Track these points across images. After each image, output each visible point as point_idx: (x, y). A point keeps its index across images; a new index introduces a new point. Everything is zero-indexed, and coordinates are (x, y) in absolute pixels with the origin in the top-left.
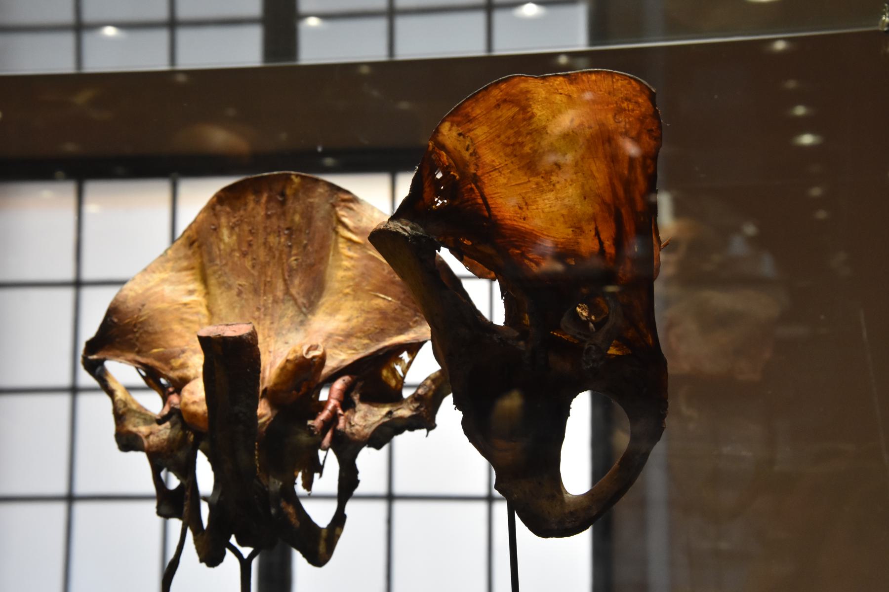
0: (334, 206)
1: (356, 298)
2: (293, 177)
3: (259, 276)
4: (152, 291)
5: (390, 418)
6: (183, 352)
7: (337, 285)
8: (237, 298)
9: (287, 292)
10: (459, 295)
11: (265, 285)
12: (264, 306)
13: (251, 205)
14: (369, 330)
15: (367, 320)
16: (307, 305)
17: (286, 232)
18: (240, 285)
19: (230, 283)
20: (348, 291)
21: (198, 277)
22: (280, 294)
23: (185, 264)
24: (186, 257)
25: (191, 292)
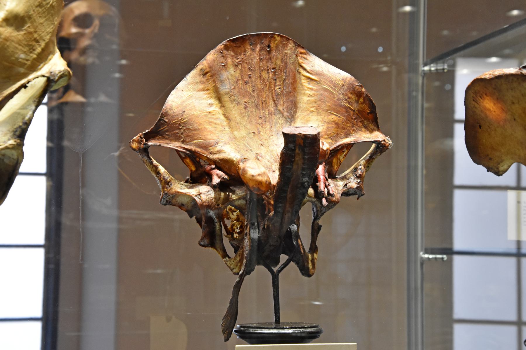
0: (297, 56)
1: (318, 114)
2: (276, 36)
4: (186, 103)
5: (346, 188)
6: (217, 143)
7: (305, 106)
8: (244, 111)
10: (157, 122)
11: (262, 103)
12: (263, 116)
14: (330, 134)
15: (328, 128)
16: (290, 117)
17: (273, 70)
18: (246, 102)
19: (239, 100)
20: (313, 109)
21: (213, 95)
23: (201, 86)
24: (202, 82)
25: (211, 105)
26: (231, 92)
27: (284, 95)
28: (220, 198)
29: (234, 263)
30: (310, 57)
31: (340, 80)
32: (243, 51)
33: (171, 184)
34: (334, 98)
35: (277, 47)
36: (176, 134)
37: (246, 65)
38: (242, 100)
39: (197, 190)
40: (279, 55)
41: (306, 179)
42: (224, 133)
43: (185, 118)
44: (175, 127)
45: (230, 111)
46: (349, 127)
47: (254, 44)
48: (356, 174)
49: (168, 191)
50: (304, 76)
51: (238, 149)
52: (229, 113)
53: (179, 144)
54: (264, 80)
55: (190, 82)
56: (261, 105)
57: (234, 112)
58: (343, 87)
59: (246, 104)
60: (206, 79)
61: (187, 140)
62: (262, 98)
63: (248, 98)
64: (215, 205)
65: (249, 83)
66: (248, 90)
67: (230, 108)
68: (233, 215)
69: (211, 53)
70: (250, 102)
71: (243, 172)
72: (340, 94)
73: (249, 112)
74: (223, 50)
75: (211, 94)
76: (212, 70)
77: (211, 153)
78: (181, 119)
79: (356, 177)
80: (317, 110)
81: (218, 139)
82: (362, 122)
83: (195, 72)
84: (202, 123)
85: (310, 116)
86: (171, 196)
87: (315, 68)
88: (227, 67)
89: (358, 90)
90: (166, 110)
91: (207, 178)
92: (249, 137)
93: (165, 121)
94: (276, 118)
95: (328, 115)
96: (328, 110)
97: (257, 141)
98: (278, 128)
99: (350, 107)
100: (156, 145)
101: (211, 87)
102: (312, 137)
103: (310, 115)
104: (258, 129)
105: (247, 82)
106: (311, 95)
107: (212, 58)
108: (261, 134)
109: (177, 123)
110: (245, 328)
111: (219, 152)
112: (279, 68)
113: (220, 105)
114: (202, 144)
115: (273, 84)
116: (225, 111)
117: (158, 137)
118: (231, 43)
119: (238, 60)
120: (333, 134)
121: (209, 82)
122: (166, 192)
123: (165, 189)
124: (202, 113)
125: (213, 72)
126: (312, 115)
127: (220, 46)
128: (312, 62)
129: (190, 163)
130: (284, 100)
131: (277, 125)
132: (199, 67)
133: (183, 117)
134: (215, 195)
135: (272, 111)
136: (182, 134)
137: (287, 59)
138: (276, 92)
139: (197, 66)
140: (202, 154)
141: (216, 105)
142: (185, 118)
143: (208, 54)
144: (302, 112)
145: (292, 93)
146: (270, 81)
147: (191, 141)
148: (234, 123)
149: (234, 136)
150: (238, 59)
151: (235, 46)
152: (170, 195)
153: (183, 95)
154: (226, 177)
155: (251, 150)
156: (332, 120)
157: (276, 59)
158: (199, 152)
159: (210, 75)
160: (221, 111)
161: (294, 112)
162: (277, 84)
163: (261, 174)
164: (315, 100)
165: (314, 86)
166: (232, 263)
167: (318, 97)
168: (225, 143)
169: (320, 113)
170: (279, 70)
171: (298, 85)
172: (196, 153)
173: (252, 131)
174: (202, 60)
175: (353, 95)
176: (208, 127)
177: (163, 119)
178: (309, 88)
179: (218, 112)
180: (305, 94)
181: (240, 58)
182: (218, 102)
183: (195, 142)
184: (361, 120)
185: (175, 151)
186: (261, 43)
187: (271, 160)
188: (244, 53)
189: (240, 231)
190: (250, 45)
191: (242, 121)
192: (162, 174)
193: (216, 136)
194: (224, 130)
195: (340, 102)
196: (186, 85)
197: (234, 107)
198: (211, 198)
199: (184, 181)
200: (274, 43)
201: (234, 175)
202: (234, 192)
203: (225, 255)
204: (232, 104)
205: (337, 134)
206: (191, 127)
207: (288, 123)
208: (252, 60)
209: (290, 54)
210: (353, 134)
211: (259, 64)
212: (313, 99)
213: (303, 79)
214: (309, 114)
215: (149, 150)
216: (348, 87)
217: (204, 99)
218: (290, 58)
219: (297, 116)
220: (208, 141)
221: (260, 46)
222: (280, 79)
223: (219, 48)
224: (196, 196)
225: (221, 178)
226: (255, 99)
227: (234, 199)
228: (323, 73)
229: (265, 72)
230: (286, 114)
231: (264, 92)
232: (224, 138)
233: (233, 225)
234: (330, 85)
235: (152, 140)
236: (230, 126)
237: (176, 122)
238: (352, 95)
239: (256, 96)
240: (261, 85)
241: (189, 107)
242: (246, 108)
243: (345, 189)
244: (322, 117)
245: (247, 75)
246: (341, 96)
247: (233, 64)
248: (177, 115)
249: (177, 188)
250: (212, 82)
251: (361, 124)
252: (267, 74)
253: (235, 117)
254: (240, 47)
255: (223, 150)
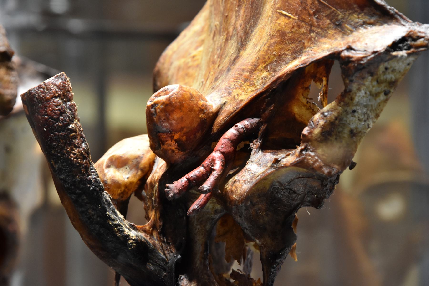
14: (269, 58)
120: (272, 57)
184: (328, 12)
205: (279, 55)
251: (328, 21)
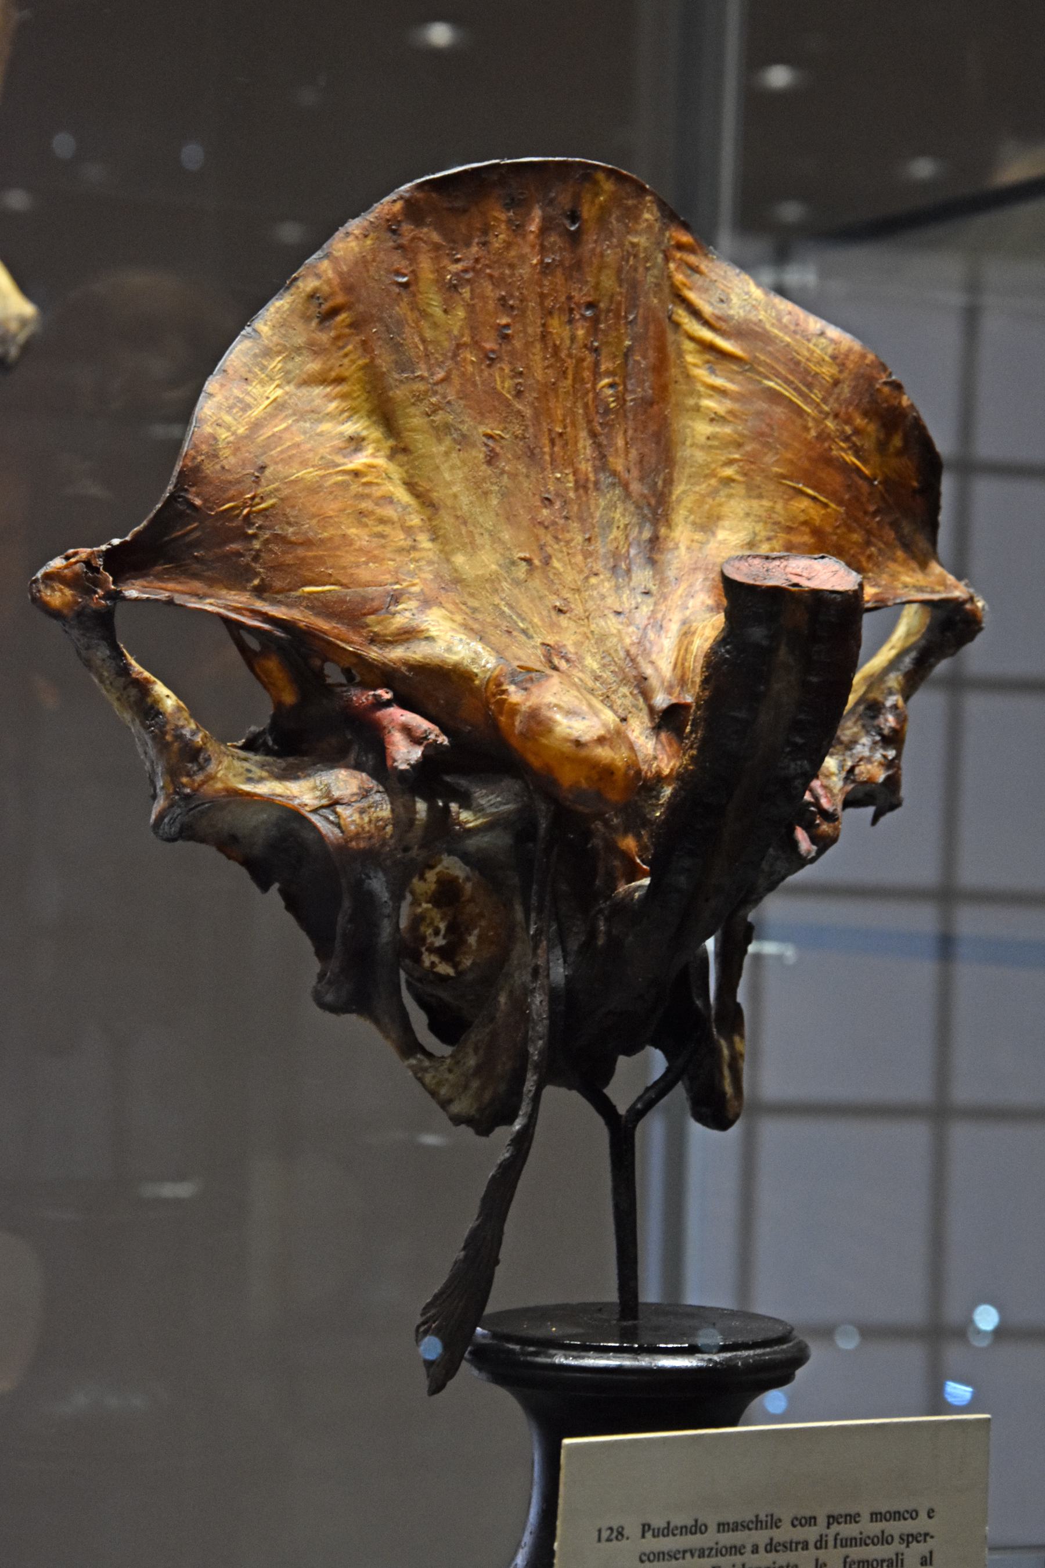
0: (667, 259)
2: (601, 176)
3: (537, 416)
4: (267, 432)
6: (396, 598)
7: (700, 456)
9: (602, 462)
10: (159, 506)
11: (553, 443)
12: (558, 495)
13: (500, 237)
16: (653, 502)
17: (588, 313)
18: (490, 437)
19: (464, 428)
20: (729, 472)
22: (586, 467)
23: (314, 366)
24: (315, 349)
25: (356, 443)
26: (435, 393)
27: (628, 414)
28: (412, 821)
29: (451, 1077)
30: (710, 265)
31: (823, 360)
32: (478, 229)
33: (208, 760)
34: (807, 429)
35: (602, 220)
36: (234, 559)
37: (488, 289)
38: (476, 428)
39: (315, 788)
40: (609, 252)
41: (801, 766)
42: (417, 561)
43: (270, 495)
44: (229, 528)
45: (433, 470)
46: (854, 543)
47: (518, 204)
48: (881, 729)
49: (196, 785)
50: (692, 338)
51: (476, 626)
52: (430, 480)
53: (243, 599)
54: (556, 350)
55: (271, 345)
56: (547, 449)
57: (447, 476)
58: (837, 390)
59: (490, 443)
60: (332, 334)
61: (278, 584)
62: (552, 421)
63: (500, 422)
64: (396, 849)
65: (499, 359)
66: (499, 387)
67: (432, 457)
68: (425, 880)
69: (350, 230)
70: (507, 436)
71: (533, 724)
72: (827, 414)
73: (505, 476)
74: (399, 222)
75: (355, 399)
76: (358, 301)
77: (374, 640)
78: (253, 498)
79: (878, 738)
80: (745, 475)
81: (396, 583)
82: (895, 525)
83: (287, 306)
84: (331, 517)
85: (723, 499)
86: (207, 805)
87: (730, 308)
88: (419, 291)
89: (887, 401)
90: (194, 458)
91: (349, 737)
92: (513, 579)
93: (192, 506)
94: (602, 503)
95: (786, 497)
96: (784, 477)
97: (541, 594)
98: (615, 545)
99: (858, 469)
100: (157, 600)
101: (354, 367)
102: (842, 601)
103: (722, 493)
104: (542, 548)
105: (492, 356)
106: (722, 417)
107: (357, 249)
108: (554, 568)
109: (237, 512)
110: (530, 1345)
111: (409, 635)
112: (611, 302)
113: (391, 442)
114: (335, 603)
115: (588, 369)
116: (411, 471)
117: (160, 568)
118: (434, 195)
119: (459, 266)
121: (346, 350)
122: (188, 791)
123: (184, 780)
124: (330, 474)
125: (361, 308)
126: (730, 496)
127: (388, 205)
128: (717, 284)
129: (281, 676)
130: (630, 432)
131: (611, 532)
132: (300, 283)
133: (260, 490)
134: (393, 810)
135: (586, 474)
136: (256, 558)
137: (636, 270)
138: (601, 400)
139: (296, 279)
140: (338, 642)
141: (374, 445)
142: (270, 495)
143: (340, 234)
144: (692, 481)
145: (656, 407)
146: (579, 354)
147: (290, 590)
148: (452, 520)
149: (456, 571)
150: (458, 261)
151: (448, 209)
152: (203, 804)
153: (248, 399)
154: (443, 740)
155: (524, 632)
156: (802, 517)
157: (601, 268)
158: (325, 633)
159: (348, 321)
160: (395, 471)
161: (665, 481)
162: (603, 368)
163: (608, 736)
164: (736, 436)
165: (731, 381)
166: (447, 1075)
167: (749, 424)
168: (427, 603)
169: (759, 487)
170: (609, 311)
171: (674, 372)
172: (314, 636)
173: (522, 555)
174: (314, 256)
175: (870, 420)
176: (356, 535)
177: (182, 494)
178: (714, 388)
179: (386, 474)
180: (697, 409)
181: (468, 259)
182: (381, 430)
183: (311, 593)
185: (221, 622)
186: (547, 201)
187: (605, 675)
188: (483, 239)
189: (447, 944)
190: (507, 207)
191: (481, 513)
192: (167, 715)
193: (389, 572)
194: (414, 548)
195: (826, 445)
196: (255, 356)
197: (447, 454)
198: (381, 823)
199: (240, 743)
200: (593, 202)
201: (470, 732)
202: (466, 803)
203: (410, 1046)
204: (440, 441)
206: (291, 530)
207: (648, 525)
208: (512, 266)
209: (645, 249)
210: (871, 571)
211: (541, 286)
212: (728, 430)
213: (691, 352)
214: (714, 493)
215: (118, 621)
216: (854, 389)
217: (330, 417)
218: (648, 265)
219: (674, 497)
220: (360, 590)
221: (543, 212)
222: (614, 349)
223: (386, 211)
224: (315, 811)
225: (425, 742)
226: (527, 426)
227: (471, 825)
228: (764, 329)
229: (559, 318)
230: (635, 487)
231: (557, 397)
232: (416, 581)
233: (417, 921)
234: (791, 377)
235: (136, 578)
236: (435, 533)
237: (232, 508)
238: (866, 421)
239: (528, 412)
240: (548, 371)
241: (279, 449)
242: (494, 460)
243: (850, 787)
244: (766, 503)
245: (491, 327)
246: (830, 424)
247: (440, 281)
248: (238, 482)
249: (230, 776)
250: (355, 348)
252: (568, 328)
253: (455, 496)
254: (465, 211)
255: (423, 627)
